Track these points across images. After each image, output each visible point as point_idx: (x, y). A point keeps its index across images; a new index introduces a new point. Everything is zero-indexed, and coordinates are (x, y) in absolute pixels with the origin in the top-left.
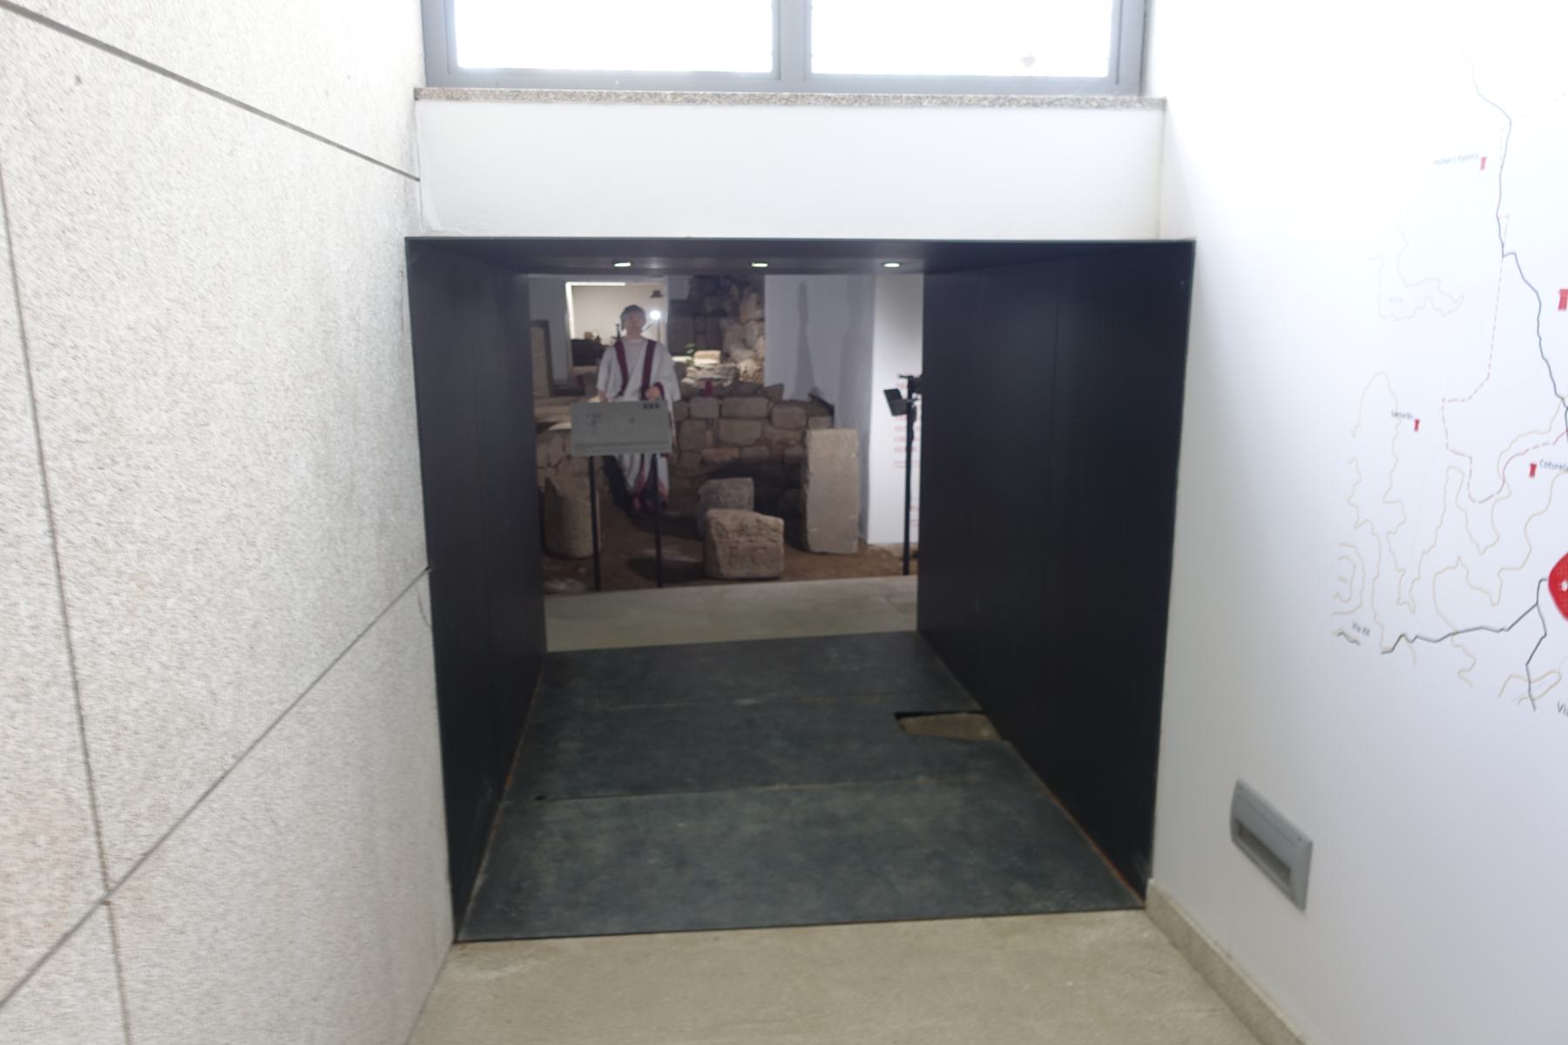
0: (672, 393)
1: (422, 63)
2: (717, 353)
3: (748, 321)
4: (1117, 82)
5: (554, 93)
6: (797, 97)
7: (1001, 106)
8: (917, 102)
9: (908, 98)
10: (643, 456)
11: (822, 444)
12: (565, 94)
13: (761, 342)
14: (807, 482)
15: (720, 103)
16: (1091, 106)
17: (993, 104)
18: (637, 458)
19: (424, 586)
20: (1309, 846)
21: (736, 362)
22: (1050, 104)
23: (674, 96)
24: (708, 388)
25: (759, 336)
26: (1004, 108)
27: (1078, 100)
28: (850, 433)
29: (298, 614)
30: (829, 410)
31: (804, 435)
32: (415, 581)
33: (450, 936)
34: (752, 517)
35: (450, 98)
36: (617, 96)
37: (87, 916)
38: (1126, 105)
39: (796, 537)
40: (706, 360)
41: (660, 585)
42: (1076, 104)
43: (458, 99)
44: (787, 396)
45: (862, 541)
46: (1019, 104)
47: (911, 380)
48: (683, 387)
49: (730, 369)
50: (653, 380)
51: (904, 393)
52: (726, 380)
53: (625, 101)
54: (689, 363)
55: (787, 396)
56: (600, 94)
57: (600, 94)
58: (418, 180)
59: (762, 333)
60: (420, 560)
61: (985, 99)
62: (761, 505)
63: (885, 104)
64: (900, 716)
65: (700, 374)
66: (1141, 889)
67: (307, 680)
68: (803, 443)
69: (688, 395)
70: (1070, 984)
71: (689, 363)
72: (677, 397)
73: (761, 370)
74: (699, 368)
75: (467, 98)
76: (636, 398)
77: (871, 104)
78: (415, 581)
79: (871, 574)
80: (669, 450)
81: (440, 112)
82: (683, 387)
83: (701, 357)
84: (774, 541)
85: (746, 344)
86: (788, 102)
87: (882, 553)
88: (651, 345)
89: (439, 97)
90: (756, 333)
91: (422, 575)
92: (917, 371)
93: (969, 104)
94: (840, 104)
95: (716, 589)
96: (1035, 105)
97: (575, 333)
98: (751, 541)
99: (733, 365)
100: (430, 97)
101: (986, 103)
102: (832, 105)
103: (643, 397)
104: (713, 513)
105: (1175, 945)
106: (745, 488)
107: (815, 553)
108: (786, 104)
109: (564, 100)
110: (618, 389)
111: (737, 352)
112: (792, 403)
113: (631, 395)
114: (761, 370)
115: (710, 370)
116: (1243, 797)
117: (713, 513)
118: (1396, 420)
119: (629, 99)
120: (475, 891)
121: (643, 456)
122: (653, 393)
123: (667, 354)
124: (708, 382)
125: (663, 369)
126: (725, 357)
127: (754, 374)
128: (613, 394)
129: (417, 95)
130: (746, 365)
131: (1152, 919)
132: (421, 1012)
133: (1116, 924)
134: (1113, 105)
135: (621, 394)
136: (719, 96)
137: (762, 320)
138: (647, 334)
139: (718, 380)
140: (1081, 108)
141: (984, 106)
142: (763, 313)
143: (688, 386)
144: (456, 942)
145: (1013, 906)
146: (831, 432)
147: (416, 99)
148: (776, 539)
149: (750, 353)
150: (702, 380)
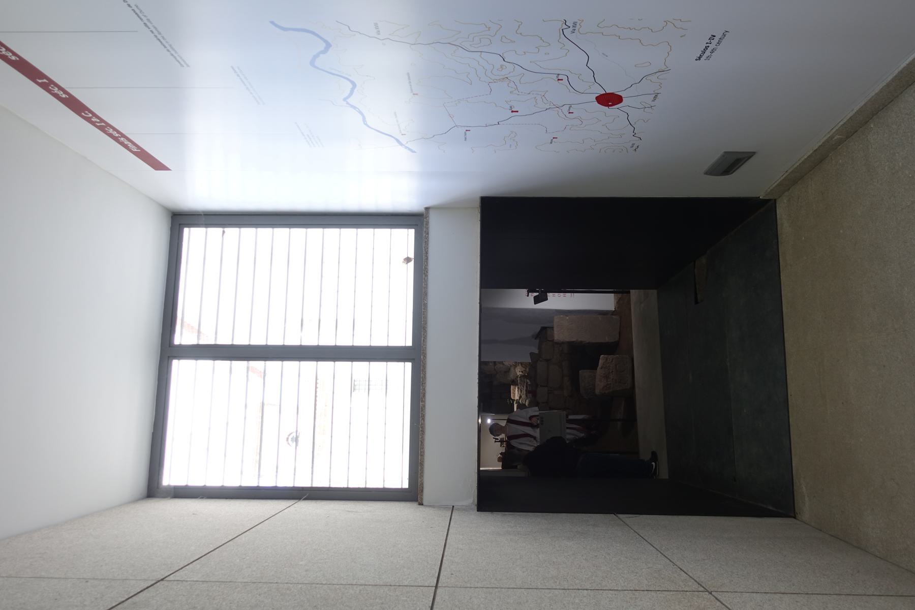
0: (534, 411)
1: (408, 502)
2: (512, 387)
3: (495, 370)
4: (417, 225)
5: (421, 449)
6: (423, 353)
7: (427, 272)
8: (426, 305)
9: (424, 309)
10: (568, 428)
11: (560, 335)
12: (421, 444)
13: (506, 363)
14: (581, 342)
15: (425, 383)
16: (428, 237)
17: (427, 276)
18: (568, 431)
19: (621, 516)
20: (725, 152)
21: (517, 377)
22: (427, 253)
23: (422, 401)
24: (532, 392)
25: (503, 364)
26: (428, 271)
27: (425, 242)
28: (556, 319)
29: (625, 548)
30: (544, 329)
31: (557, 343)
32: (620, 519)
33: (793, 519)
34: (599, 371)
35: (422, 491)
36: (422, 424)
37: (713, 596)
38: (427, 223)
39: (611, 348)
40: (516, 394)
41: (636, 420)
42: (427, 243)
43: (423, 488)
44: (536, 351)
45: (613, 313)
46: (427, 265)
47: (528, 292)
48: (531, 405)
49: (521, 380)
50: (528, 421)
51: (536, 294)
52: (527, 383)
53: (424, 421)
54: (518, 402)
55: (536, 351)
56: (421, 431)
57: (421, 431)
58: (453, 506)
59: (502, 363)
60: (612, 517)
61: (425, 279)
62: (594, 366)
63: (426, 318)
64: (696, 302)
65: (524, 396)
66: (765, 202)
67: (652, 548)
68: (561, 344)
69: (534, 403)
70: (803, 238)
71: (518, 402)
72: (536, 408)
73: (521, 364)
74: (520, 397)
75: (422, 484)
76: (538, 430)
77: (426, 324)
78: (620, 519)
79: (630, 309)
80: (565, 413)
81: (427, 495)
82: (531, 405)
83: (514, 396)
84: (612, 359)
85: (507, 371)
86: (425, 356)
87: (619, 303)
88: (509, 421)
89: (422, 495)
90: (501, 366)
91: (617, 516)
92: (525, 291)
93: (427, 285)
94: (426, 336)
95: (637, 390)
96: (427, 259)
97: (498, 467)
98: (612, 372)
99: (519, 379)
100: (422, 499)
101: (426, 278)
102: (426, 339)
103: (537, 426)
104: (597, 392)
105: (789, 189)
106: (584, 374)
107: (619, 339)
108: (426, 357)
109: (423, 445)
110: (532, 439)
111: (512, 376)
112: (540, 348)
113: (537, 433)
114: (521, 364)
115: (521, 391)
116: (707, 173)
117: (597, 392)
118: (553, 143)
119: (423, 419)
120: (774, 509)
121: (568, 428)
122: (534, 421)
123: (513, 414)
124: (528, 392)
125: (524, 416)
126: (514, 383)
127: (524, 367)
128: (535, 442)
129: (421, 504)
130: (519, 371)
131: (779, 197)
132: (821, 530)
133: (781, 211)
134: (428, 228)
135: (535, 438)
136: (422, 384)
137: (495, 363)
138: (503, 423)
139: (527, 387)
140: (428, 240)
141: (427, 279)
142: (491, 362)
143: (530, 403)
144: (795, 518)
145: (776, 258)
146: (555, 329)
147: (422, 505)
148: (611, 359)
149: (512, 369)
150: (526, 396)
